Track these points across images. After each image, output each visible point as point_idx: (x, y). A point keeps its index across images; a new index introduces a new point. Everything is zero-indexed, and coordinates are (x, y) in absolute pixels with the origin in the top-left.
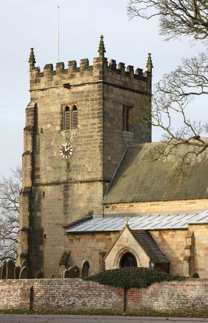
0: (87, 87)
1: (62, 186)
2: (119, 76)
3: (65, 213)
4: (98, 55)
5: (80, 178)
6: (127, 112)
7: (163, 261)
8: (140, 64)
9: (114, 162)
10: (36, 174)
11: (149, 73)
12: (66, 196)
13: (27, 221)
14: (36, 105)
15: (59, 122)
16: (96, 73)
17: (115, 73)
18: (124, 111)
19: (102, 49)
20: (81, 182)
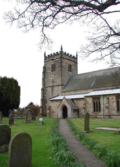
0: (58, 59)
1: (51, 87)
2: (67, 57)
3: (52, 95)
4: (60, 50)
5: (56, 85)
6: (70, 67)
7: (76, 109)
8: (74, 54)
9: (65, 80)
10: (45, 84)
11: (77, 57)
12: (52, 90)
13: (42, 97)
14: (45, 66)
15: (51, 70)
16: (60, 55)
17: (66, 56)
18: (69, 66)
19: (62, 49)
20: (56, 86)
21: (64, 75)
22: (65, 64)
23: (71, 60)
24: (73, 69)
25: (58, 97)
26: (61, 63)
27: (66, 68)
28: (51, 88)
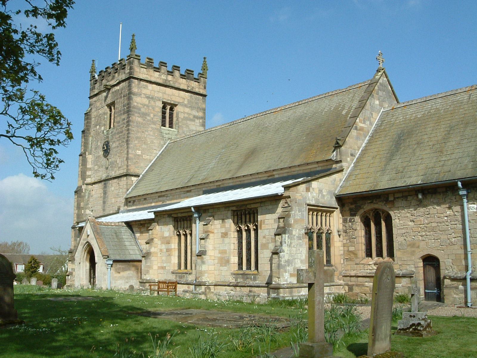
1: (103, 183)
12: (105, 193)
18: (164, 107)
21: (137, 138)
22: (146, 101)
23: (177, 85)
24: (181, 116)
25: (118, 214)
26: (129, 99)
27: (152, 115)
28: (101, 185)
